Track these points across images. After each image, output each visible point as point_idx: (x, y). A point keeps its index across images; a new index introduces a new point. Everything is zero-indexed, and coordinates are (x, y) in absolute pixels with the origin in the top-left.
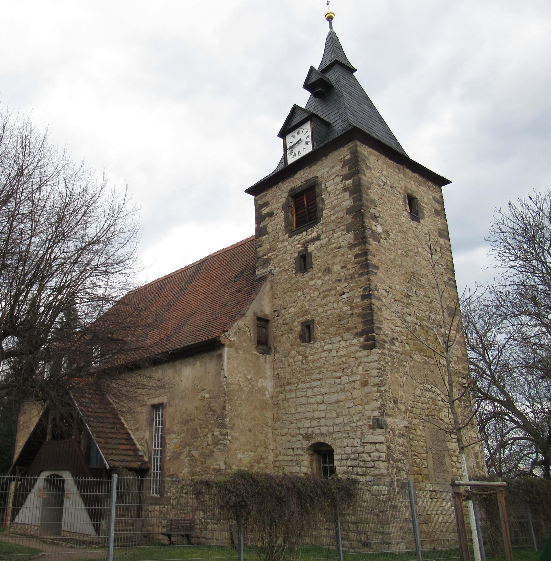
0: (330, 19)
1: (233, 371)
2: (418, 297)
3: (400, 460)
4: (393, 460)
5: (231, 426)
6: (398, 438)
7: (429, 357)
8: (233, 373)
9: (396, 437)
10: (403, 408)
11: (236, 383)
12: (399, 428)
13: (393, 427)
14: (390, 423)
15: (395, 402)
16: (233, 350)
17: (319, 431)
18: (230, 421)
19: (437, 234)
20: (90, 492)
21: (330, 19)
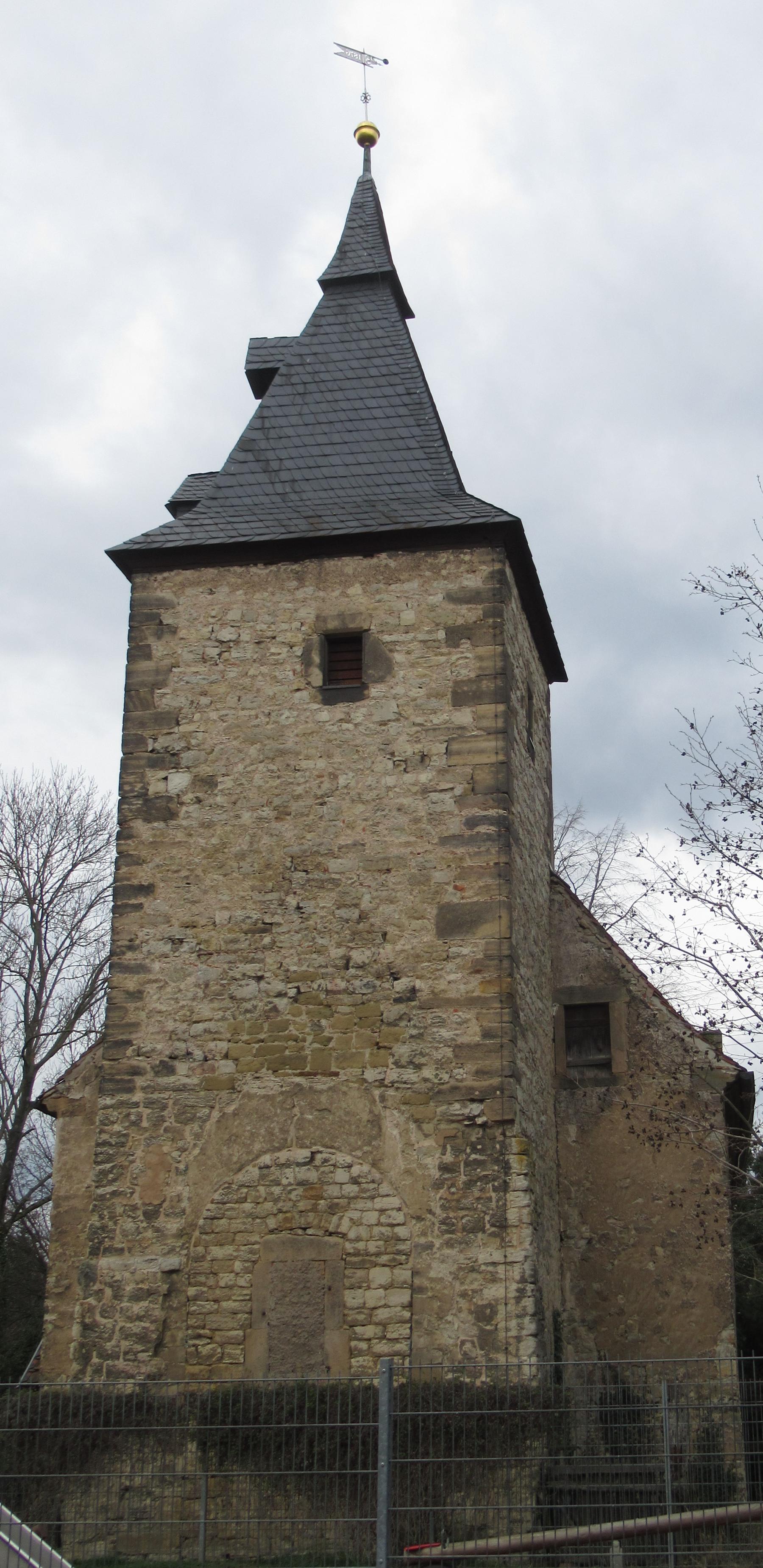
0: (367, 141)
1: (76, 1169)
2: (305, 920)
3: (126, 1353)
4: (100, 1356)
5: (60, 1290)
6: (129, 1301)
7: (315, 1074)
8: (74, 1173)
9: (126, 1299)
10: (173, 1225)
11: (80, 1193)
12: (138, 1277)
13: (118, 1277)
14: (109, 1269)
15: (151, 1215)
16: (79, 1119)
17: (396, 1271)
18: (58, 1280)
19: (445, 703)
20: (755, 1424)
21: (367, 141)
